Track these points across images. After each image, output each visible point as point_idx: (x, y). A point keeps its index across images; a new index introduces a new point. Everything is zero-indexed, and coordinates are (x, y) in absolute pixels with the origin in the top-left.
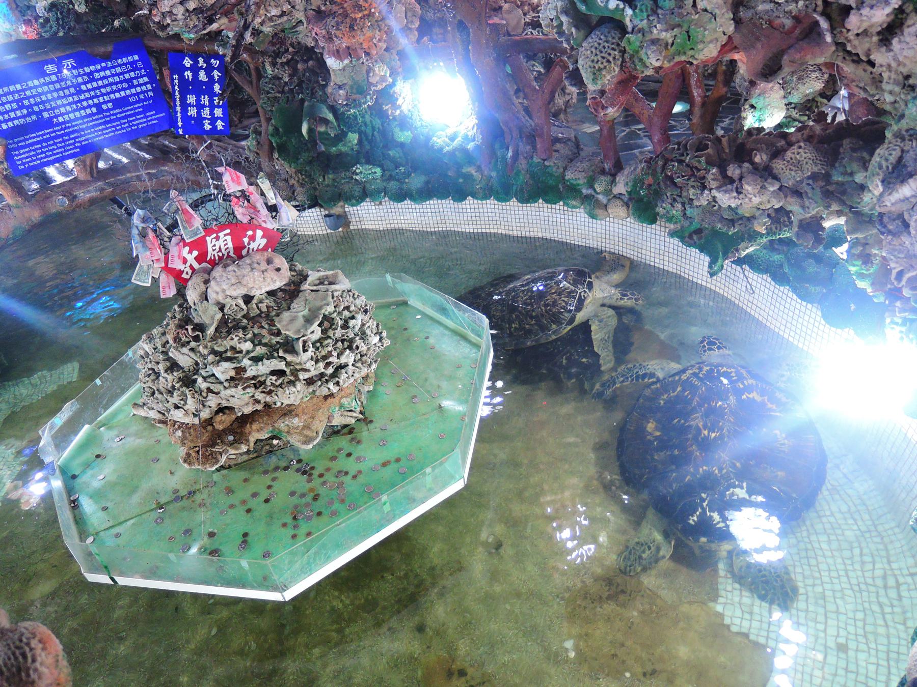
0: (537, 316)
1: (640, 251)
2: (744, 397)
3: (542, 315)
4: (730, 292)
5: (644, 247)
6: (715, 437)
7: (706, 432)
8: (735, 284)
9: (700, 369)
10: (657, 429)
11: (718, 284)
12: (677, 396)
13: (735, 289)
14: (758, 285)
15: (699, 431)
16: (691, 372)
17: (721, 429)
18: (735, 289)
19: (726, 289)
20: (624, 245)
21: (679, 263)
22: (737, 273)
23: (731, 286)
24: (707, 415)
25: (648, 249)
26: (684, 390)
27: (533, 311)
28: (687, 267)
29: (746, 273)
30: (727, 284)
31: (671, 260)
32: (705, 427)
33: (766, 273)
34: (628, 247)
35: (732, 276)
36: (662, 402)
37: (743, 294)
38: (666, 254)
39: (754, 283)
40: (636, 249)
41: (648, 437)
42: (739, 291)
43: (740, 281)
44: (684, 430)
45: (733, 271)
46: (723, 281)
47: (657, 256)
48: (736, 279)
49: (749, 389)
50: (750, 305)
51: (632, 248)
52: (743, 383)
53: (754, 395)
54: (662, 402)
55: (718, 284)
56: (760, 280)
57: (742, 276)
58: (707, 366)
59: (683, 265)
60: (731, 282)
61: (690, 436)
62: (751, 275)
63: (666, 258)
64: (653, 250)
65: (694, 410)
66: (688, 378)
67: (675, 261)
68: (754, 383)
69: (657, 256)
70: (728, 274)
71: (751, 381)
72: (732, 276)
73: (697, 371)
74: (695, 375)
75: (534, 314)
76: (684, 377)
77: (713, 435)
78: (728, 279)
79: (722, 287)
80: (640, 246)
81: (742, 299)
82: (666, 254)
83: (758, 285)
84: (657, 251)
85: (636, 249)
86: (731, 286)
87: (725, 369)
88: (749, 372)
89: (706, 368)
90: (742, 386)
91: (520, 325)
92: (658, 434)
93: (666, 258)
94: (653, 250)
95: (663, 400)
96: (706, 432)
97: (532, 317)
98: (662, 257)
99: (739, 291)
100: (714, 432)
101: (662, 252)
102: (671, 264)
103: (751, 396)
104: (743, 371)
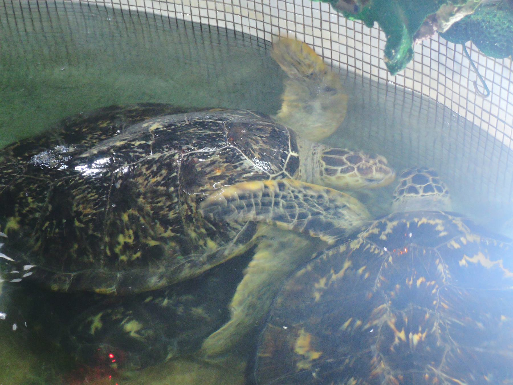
0: (177, 221)
1: (275, 21)
2: (463, 262)
3: (189, 218)
4: (449, 93)
5: (283, 14)
6: (420, 342)
7: (402, 335)
8: (457, 78)
9: (382, 227)
10: (313, 347)
11: (426, 80)
12: (345, 278)
13: (456, 88)
14: (498, 79)
15: (390, 335)
16: (365, 234)
17: (428, 325)
18: (456, 88)
19: (441, 89)
20: (245, 12)
21: (351, 42)
22: (459, 57)
23: (449, 83)
24: (398, 305)
25: (291, 17)
26: (355, 266)
27: (171, 208)
28: (367, 49)
29: (474, 56)
30: (442, 79)
31: (335, 37)
32: (400, 325)
33: (507, 56)
34: (252, 14)
35: (450, 64)
36: (317, 296)
37: (471, 97)
38: (326, 25)
39: (490, 75)
40: (267, 19)
41: (300, 365)
42: (464, 92)
43: (465, 72)
44: (359, 340)
45: (451, 54)
46: (434, 74)
47: (308, 30)
48: (457, 68)
49: (469, 249)
50: (486, 116)
51: (260, 16)
52: (458, 241)
53: (479, 258)
54: (317, 296)
55: (426, 80)
56: (499, 69)
57: (466, 62)
58: (391, 220)
59: (359, 46)
60: (449, 74)
61: (373, 348)
62: (483, 59)
63: (326, 34)
64: (299, 19)
65: (377, 298)
66: (362, 246)
67: (343, 40)
68: (478, 239)
69: (308, 30)
70: (443, 59)
71: (471, 238)
72: (450, 64)
73: (376, 231)
74: (373, 238)
75: (171, 215)
76: (355, 245)
77: (416, 338)
78: (442, 70)
79: (434, 84)
80: (274, 12)
81: (471, 107)
82: (326, 25)
83: (498, 79)
84: (308, 21)
85: (267, 19)
86: (449, 83)
87: (424, 220)
88: (467, 222)
89: (390, 226)
90: (456, 246)
91: (137, 237)
92: (315, 355)
93: (326, 34)
94: (299, 19)
95: (319, 290)
96: (402, 335)
97: (166, 223)
98: (317, 33)
99: (464, 92)
100: (416, 332)
101: (317, 23)
102: (335, 46)
103: (474, 260)
104: (458, 222)
